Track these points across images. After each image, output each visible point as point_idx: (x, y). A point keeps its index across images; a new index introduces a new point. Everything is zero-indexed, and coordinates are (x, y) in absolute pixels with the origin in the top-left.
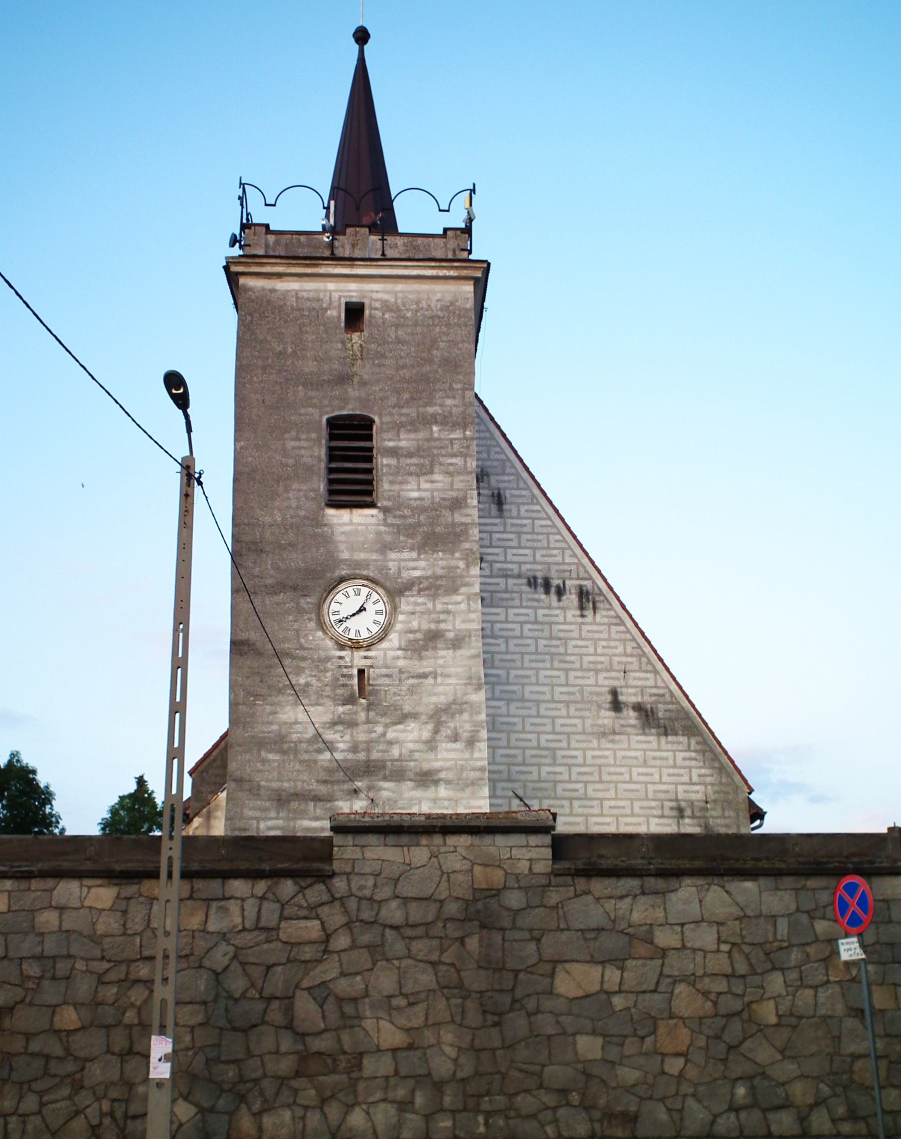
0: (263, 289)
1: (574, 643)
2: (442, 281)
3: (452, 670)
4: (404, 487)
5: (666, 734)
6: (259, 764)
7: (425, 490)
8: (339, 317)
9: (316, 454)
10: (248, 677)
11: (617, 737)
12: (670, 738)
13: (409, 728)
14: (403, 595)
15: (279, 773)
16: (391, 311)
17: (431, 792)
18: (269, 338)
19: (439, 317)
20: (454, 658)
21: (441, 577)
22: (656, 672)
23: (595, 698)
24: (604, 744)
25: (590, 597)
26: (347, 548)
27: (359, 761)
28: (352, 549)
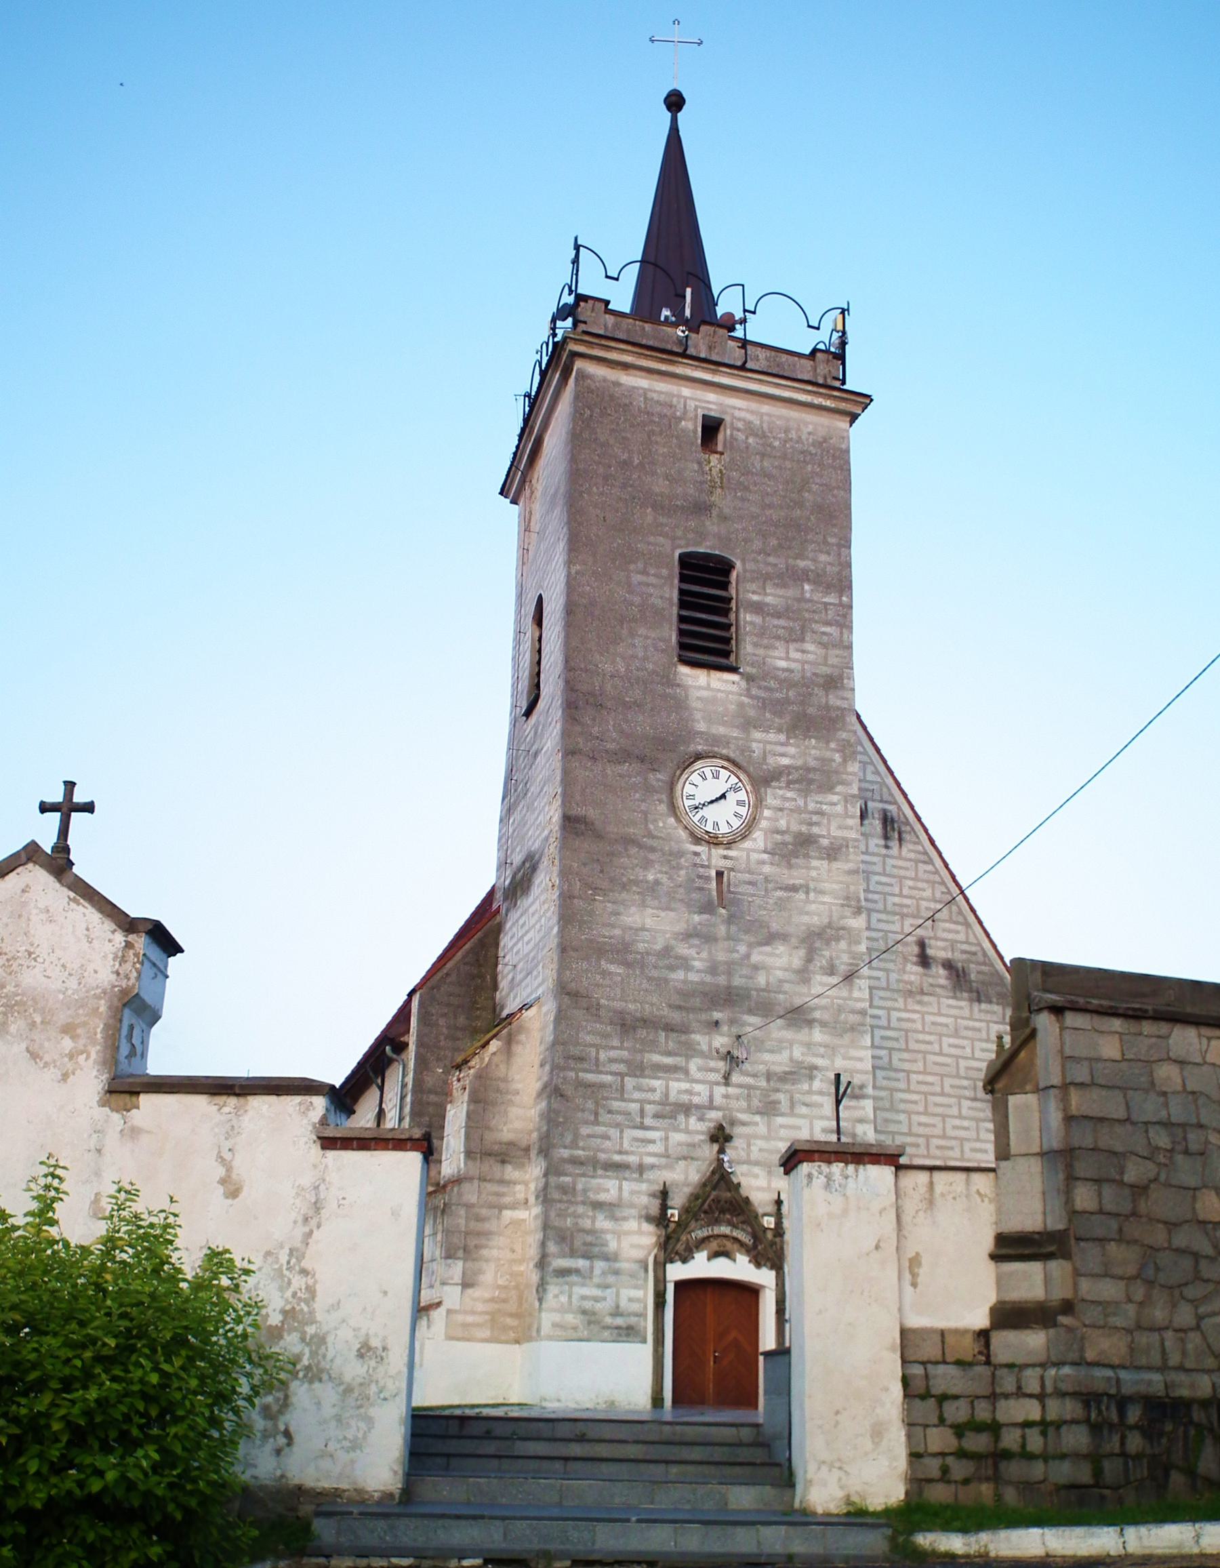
0: (605, 380)
1: (877, 878)
2: (814, 411)
3: (826, 886)
4: (771, 653)
5: (979, 1001)
6: (598, 977)
7: (795, 661)
8: (695, 431)
9: (667, 596)
10: (585, 864)
11: (926, 998)
12: (983, 1006)
13: (777, 952)
14: (769, 786)
15: (623, 990)
16: (756, 435)
17: (803, 1035)
18: (612, 441)
19: (811, 454)
20: (829, 871)
21: (815, 769)
22: (967, 925)
24: (912, 1005)
26: (703, 718)
27: (718, 986)
28: (709, 720)
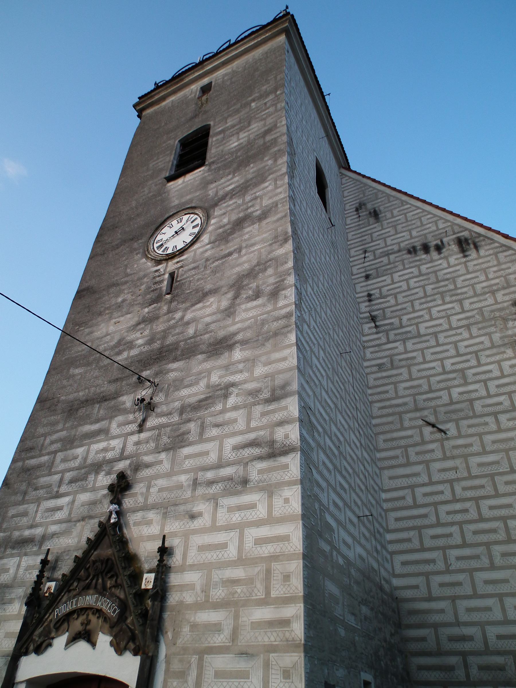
23: (497, 314)
25: (470, 241)
